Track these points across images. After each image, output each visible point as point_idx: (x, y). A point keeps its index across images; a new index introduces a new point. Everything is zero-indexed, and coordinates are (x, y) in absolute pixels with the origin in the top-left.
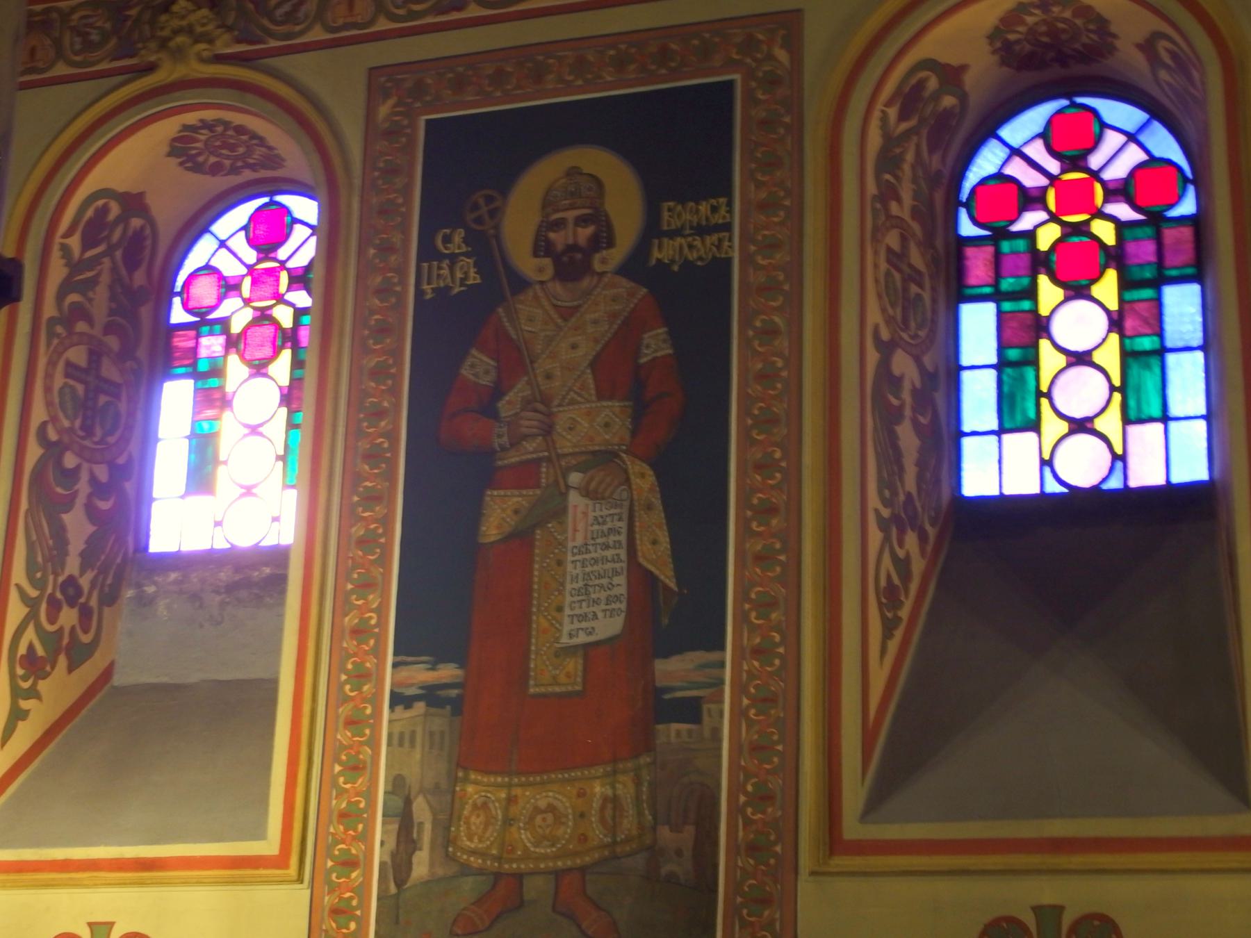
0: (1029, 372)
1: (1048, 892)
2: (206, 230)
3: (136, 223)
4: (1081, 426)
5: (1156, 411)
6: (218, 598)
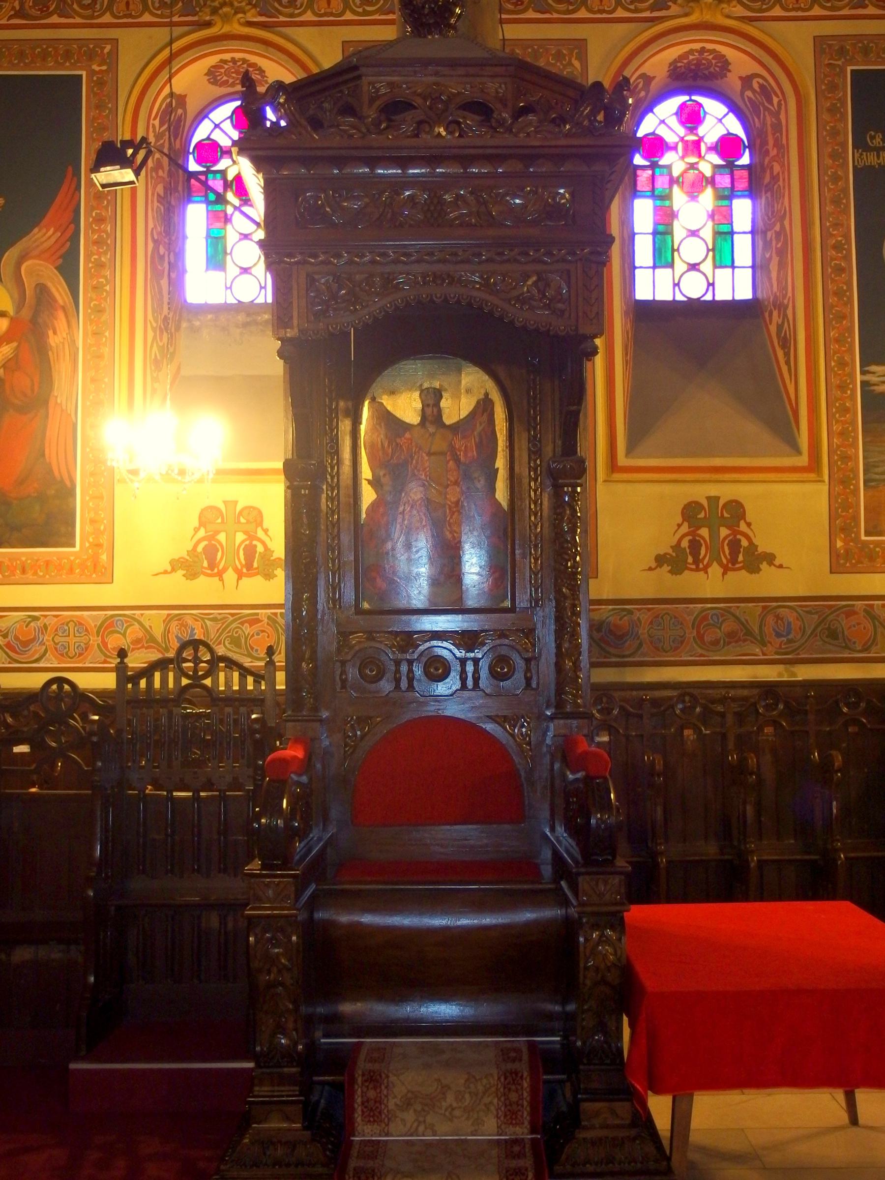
0: (669, 238)
1: (713, 490)
2: (206, 116)
3: (180, 111)
5: (729, 264)
6: (238, 331)
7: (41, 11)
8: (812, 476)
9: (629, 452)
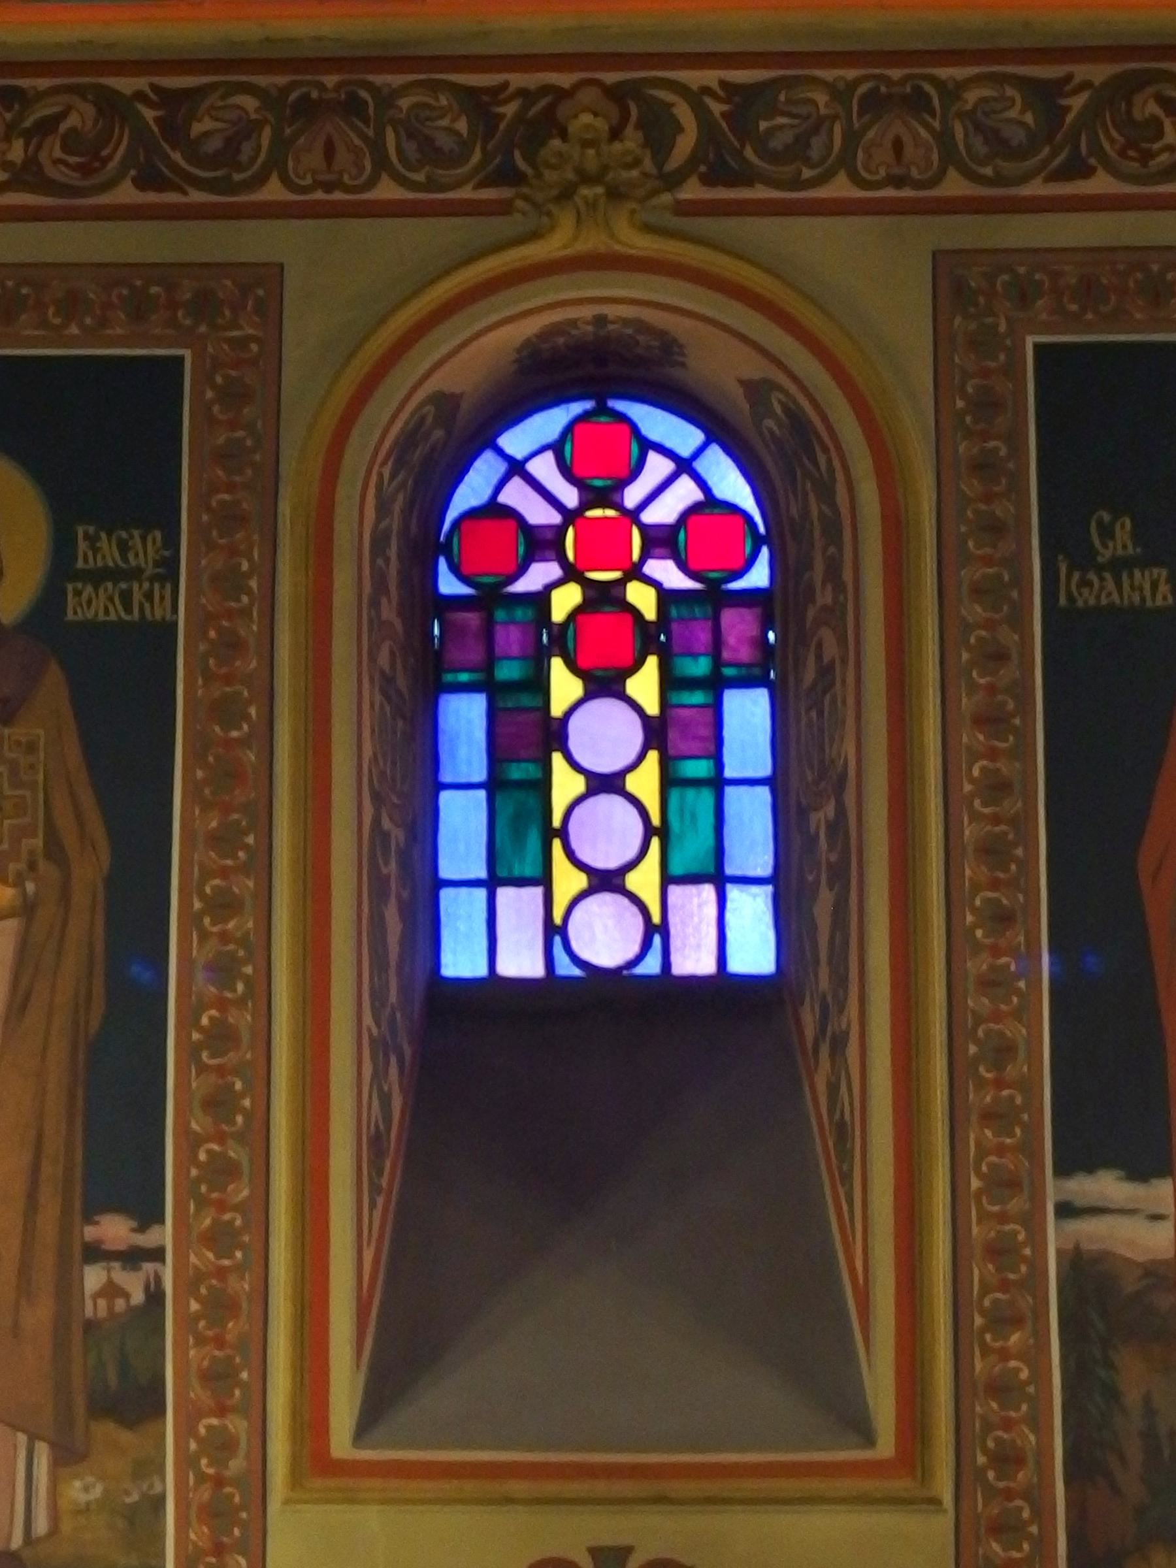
4: (607, 881)
7: (85, 170)
8: (900, 1485)
9: (364, 1429)
